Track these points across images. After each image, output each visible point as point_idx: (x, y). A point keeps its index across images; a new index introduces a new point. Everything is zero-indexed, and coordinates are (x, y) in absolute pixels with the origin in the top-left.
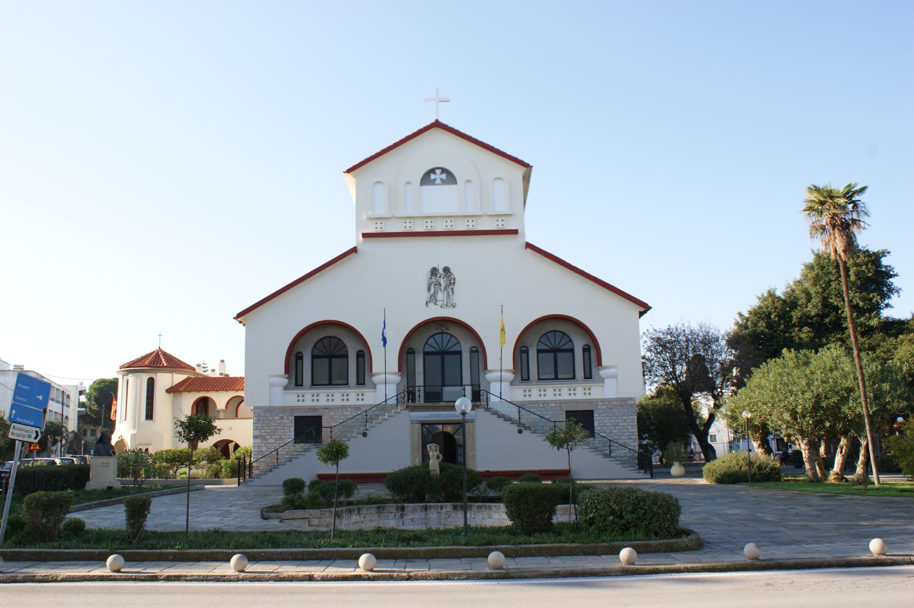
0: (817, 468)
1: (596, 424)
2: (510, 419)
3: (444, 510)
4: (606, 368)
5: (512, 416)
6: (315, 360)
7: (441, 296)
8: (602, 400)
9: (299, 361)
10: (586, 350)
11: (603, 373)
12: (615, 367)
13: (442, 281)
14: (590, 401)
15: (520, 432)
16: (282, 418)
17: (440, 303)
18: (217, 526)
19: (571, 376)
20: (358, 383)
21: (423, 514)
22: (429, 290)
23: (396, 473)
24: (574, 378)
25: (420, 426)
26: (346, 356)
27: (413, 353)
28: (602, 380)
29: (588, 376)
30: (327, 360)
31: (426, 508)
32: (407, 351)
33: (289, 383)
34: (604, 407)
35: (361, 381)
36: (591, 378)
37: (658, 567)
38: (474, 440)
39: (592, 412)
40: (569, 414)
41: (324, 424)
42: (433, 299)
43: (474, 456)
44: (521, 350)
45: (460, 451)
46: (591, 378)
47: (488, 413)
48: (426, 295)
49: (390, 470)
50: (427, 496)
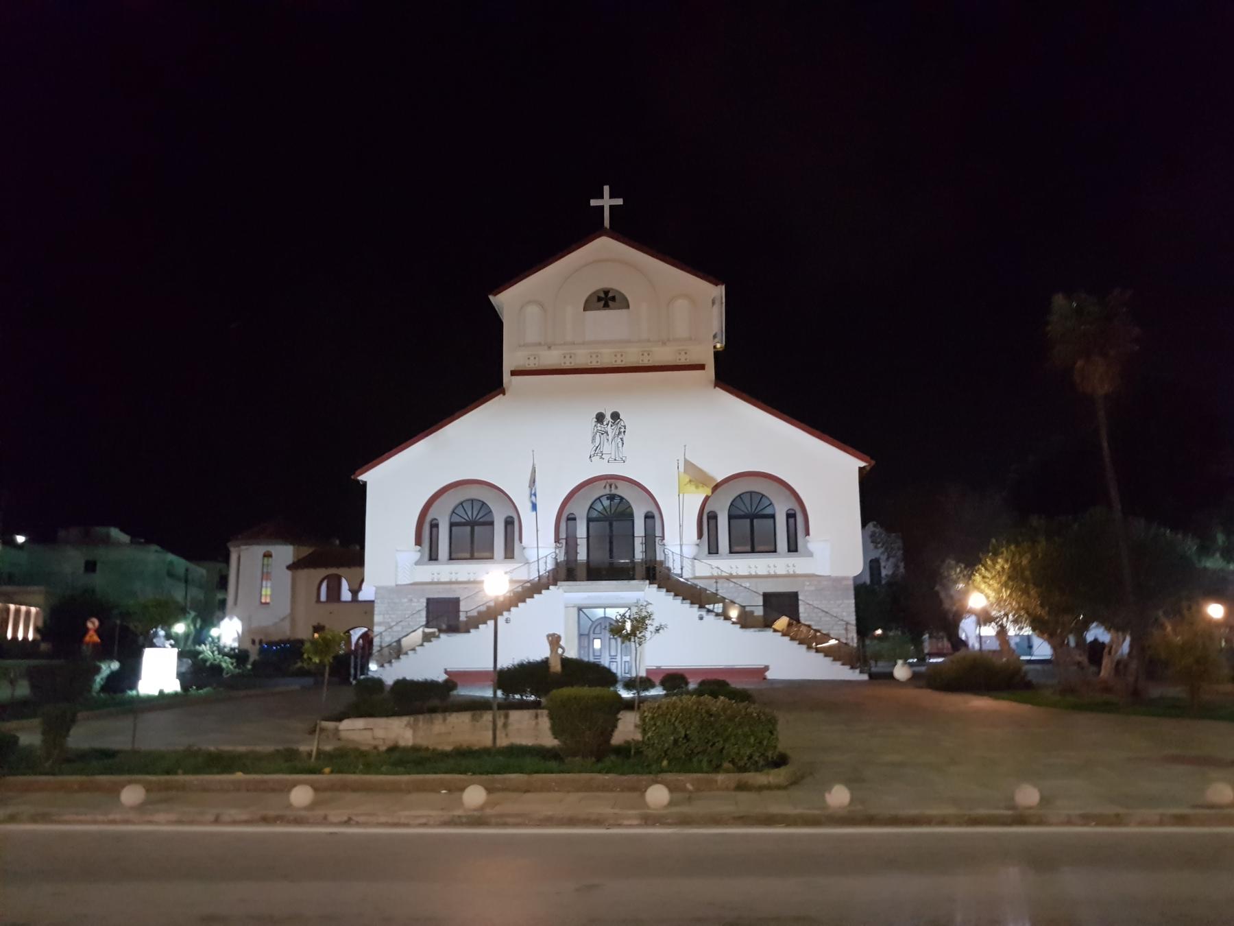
0: (940, 660)
1: (801, 609)
6: (591, 524)
7: (607, 448)
9: (434, 530)
10: (791, 516)
13: (609, 429)
16: (411, 600)
17: (606, 457)
19: (772, 548)
20: (789, 551)
22: (594, 439)
24: (775, 551)
25: (576, 610)
26: (492, 523)
27: (574, 519)
29: (793, 548)
30: (468, 528)
32: (565, 518)
33: (422, 556)
35: (793, 548)
36: (796, 551)
37: (258, 748)
40: (767, 597)
41: (462, 608)
42: (598, 452)
44: (707, 520)
46: (796, 551)
48: (590, 448)
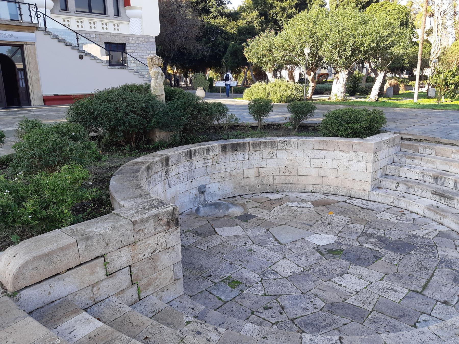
2: (71, 45)
3: (211, 154)
4: (134, 8)
5: (72, 42)
8: (132, 36)
11: (129, 12)
12: (141, 9)
14: (124, 36)
15: (81, 57)
18: (329, 154)
21: (188, 164)
23: (93, 96)
24: (105, 13)
28: (128, 19)
31: (190, 154)
34: (134, 42)
38: (36, 63)
39: (125, 44)
43: (38, 80)
45: (20, 75)
47: (49, 36)
49: (89, 92)
50: (160, 136)
